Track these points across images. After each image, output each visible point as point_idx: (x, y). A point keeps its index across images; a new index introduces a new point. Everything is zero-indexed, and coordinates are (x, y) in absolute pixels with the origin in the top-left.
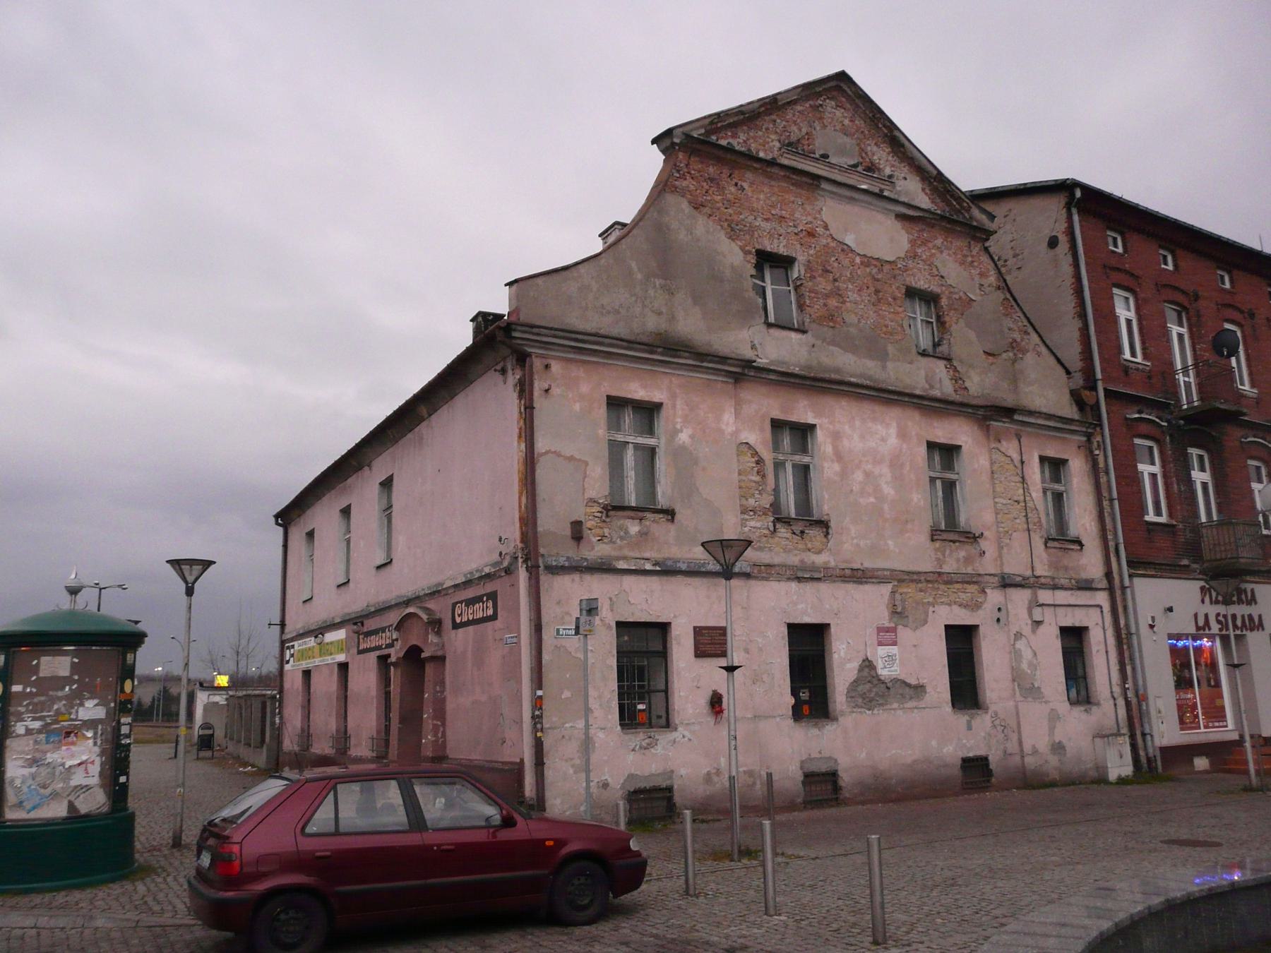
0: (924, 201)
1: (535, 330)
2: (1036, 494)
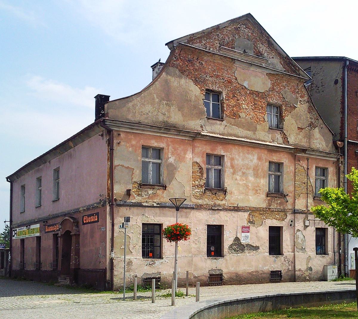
0: (280, 67)
1: (114, 122)
2: (312, 180)
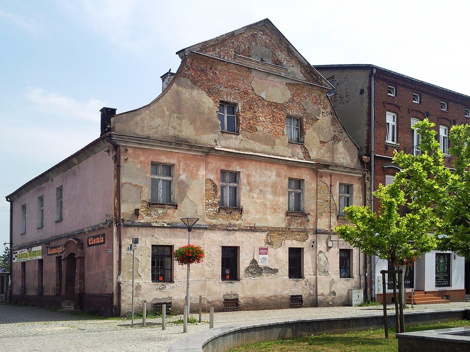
1: (121, 137)
